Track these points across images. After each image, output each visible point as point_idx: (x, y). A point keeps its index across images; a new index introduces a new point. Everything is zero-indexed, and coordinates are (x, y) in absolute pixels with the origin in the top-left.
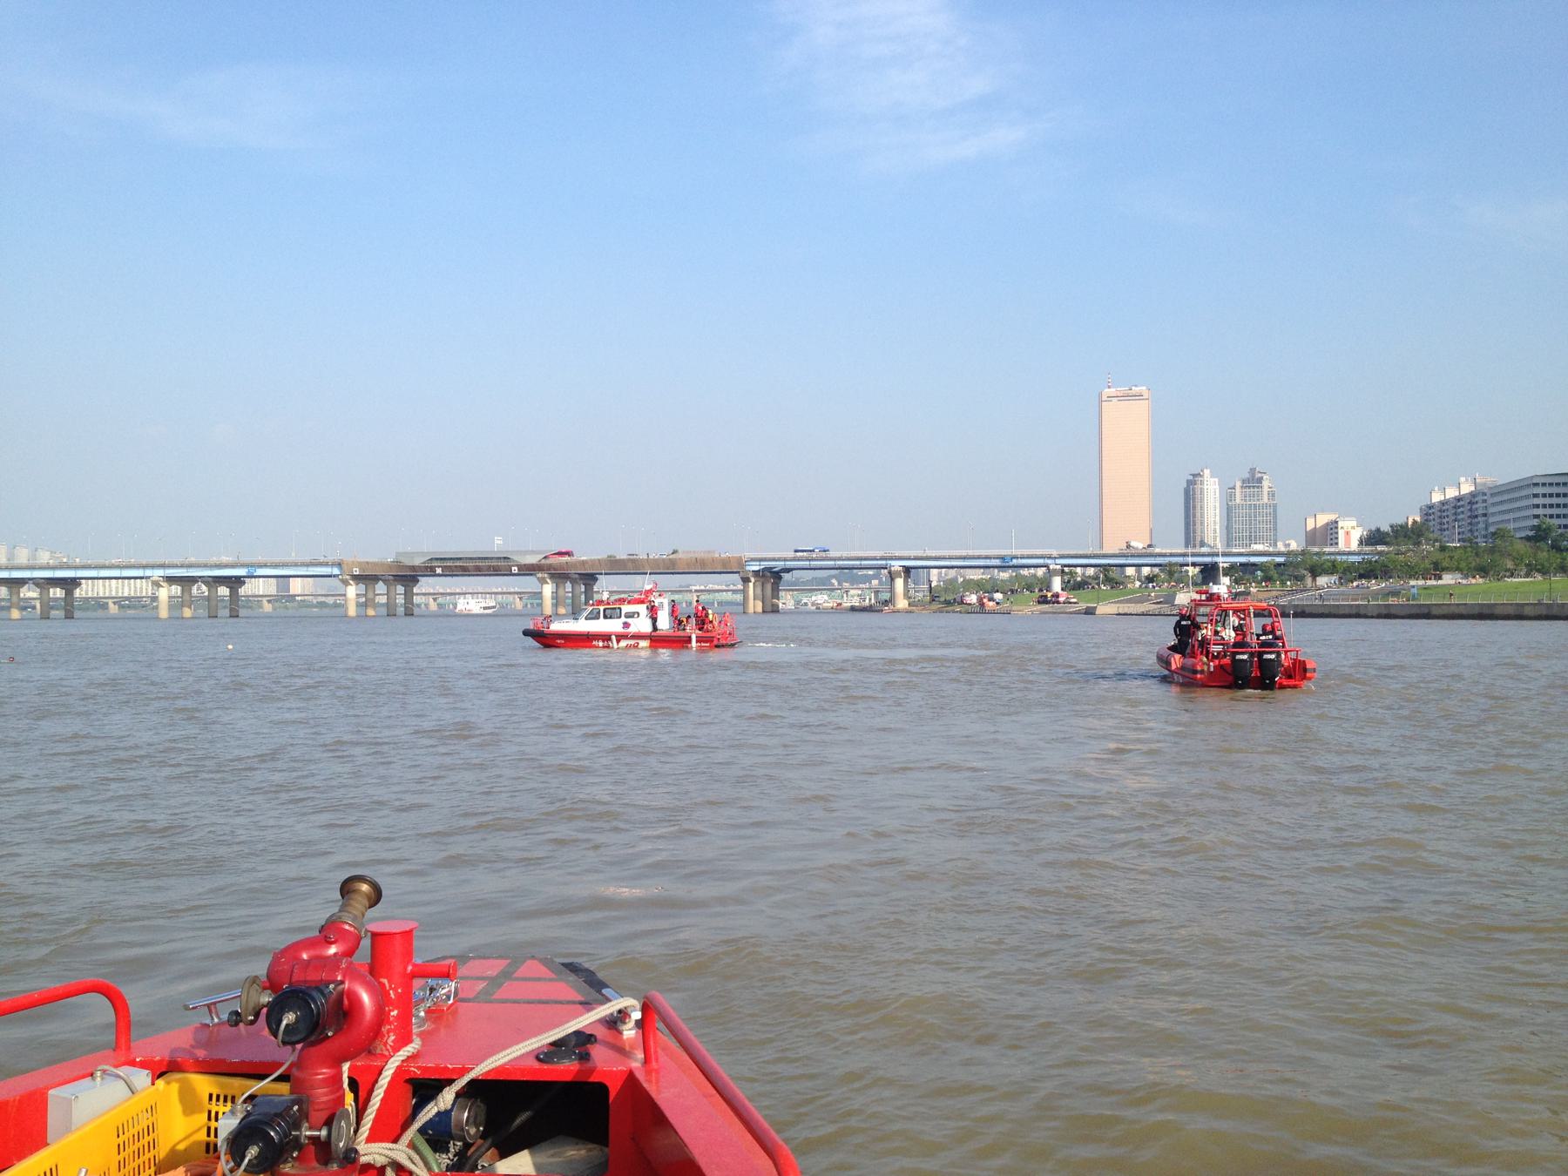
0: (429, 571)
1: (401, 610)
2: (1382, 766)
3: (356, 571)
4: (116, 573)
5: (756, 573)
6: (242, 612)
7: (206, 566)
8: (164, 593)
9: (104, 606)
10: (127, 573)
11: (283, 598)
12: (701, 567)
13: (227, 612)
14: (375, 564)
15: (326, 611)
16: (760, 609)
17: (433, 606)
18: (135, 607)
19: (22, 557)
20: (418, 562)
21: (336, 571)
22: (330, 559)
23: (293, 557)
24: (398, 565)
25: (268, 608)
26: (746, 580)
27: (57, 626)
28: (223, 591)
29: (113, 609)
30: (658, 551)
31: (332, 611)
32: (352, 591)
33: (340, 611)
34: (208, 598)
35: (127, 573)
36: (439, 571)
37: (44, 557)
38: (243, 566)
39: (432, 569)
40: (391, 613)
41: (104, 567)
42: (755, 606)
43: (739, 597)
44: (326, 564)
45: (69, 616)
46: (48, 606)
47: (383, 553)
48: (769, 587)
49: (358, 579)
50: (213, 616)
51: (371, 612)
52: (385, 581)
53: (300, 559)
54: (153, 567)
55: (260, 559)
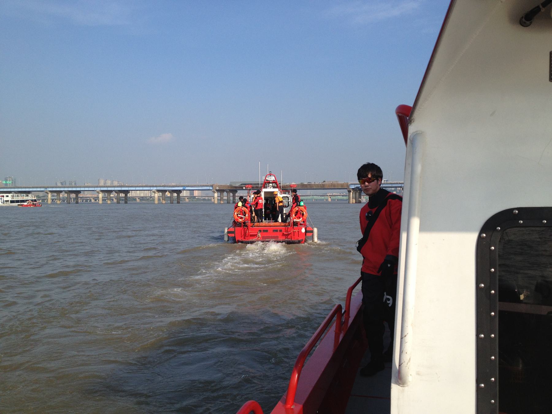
0: (241, 188)
1: (231, 202)
2: (90, 291)
3: (218, 188)
4: (141, 189)
5: (353, 189)
6: (181, 202)
7: (170, 186)
8: (157, 195)
9: (135, 200)
10: (137, 189)
11: (192, 197)
12: (333, 187)
13: (176, 202)
14: (224, 186)
15: (205, 202)
16: (354, 202)
17: (330, 200)
18: (145, 200)
19: (109, 183)
20: (237, 185)
21: (211, 188)
22: (209, 184)
23: (198, 184)
24: (231, 186)
25: (187, 200)
26: (349, 192)
27: (122, 205)
28: (175, 195)
29: (138, 200)
30: (319, 182)
31: (207, 202)
32: (216, 195)
33: (152, 202)
34: (170, 197)
35: (137, 189)
36: (244, 188)
37: (116, 183)
38: (181, 186)
39: (242, 188)
40: (228, 203)
41: (137, 187)
42: (352, 201)
43: (345, 198)
44: (208, 186)
45: (126, 203)
46: (119, 199)
47: (226, 182)
48: (358, 194)
49: (218, 191)
50: (172, 203)
51: (222, 202)
52: (227, 192)
53: (200, 184)
54: (153, 186)
55: (187, 184)
